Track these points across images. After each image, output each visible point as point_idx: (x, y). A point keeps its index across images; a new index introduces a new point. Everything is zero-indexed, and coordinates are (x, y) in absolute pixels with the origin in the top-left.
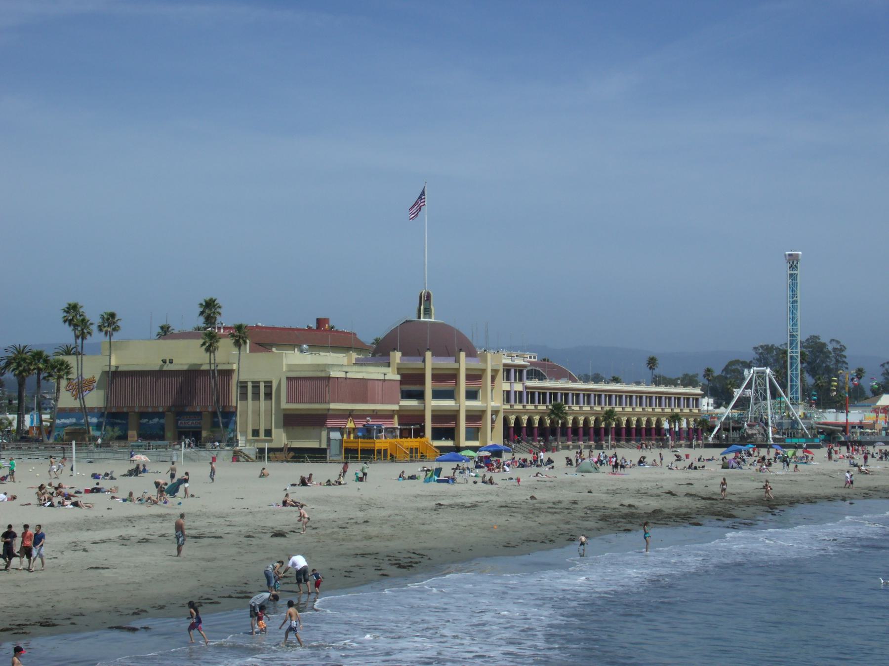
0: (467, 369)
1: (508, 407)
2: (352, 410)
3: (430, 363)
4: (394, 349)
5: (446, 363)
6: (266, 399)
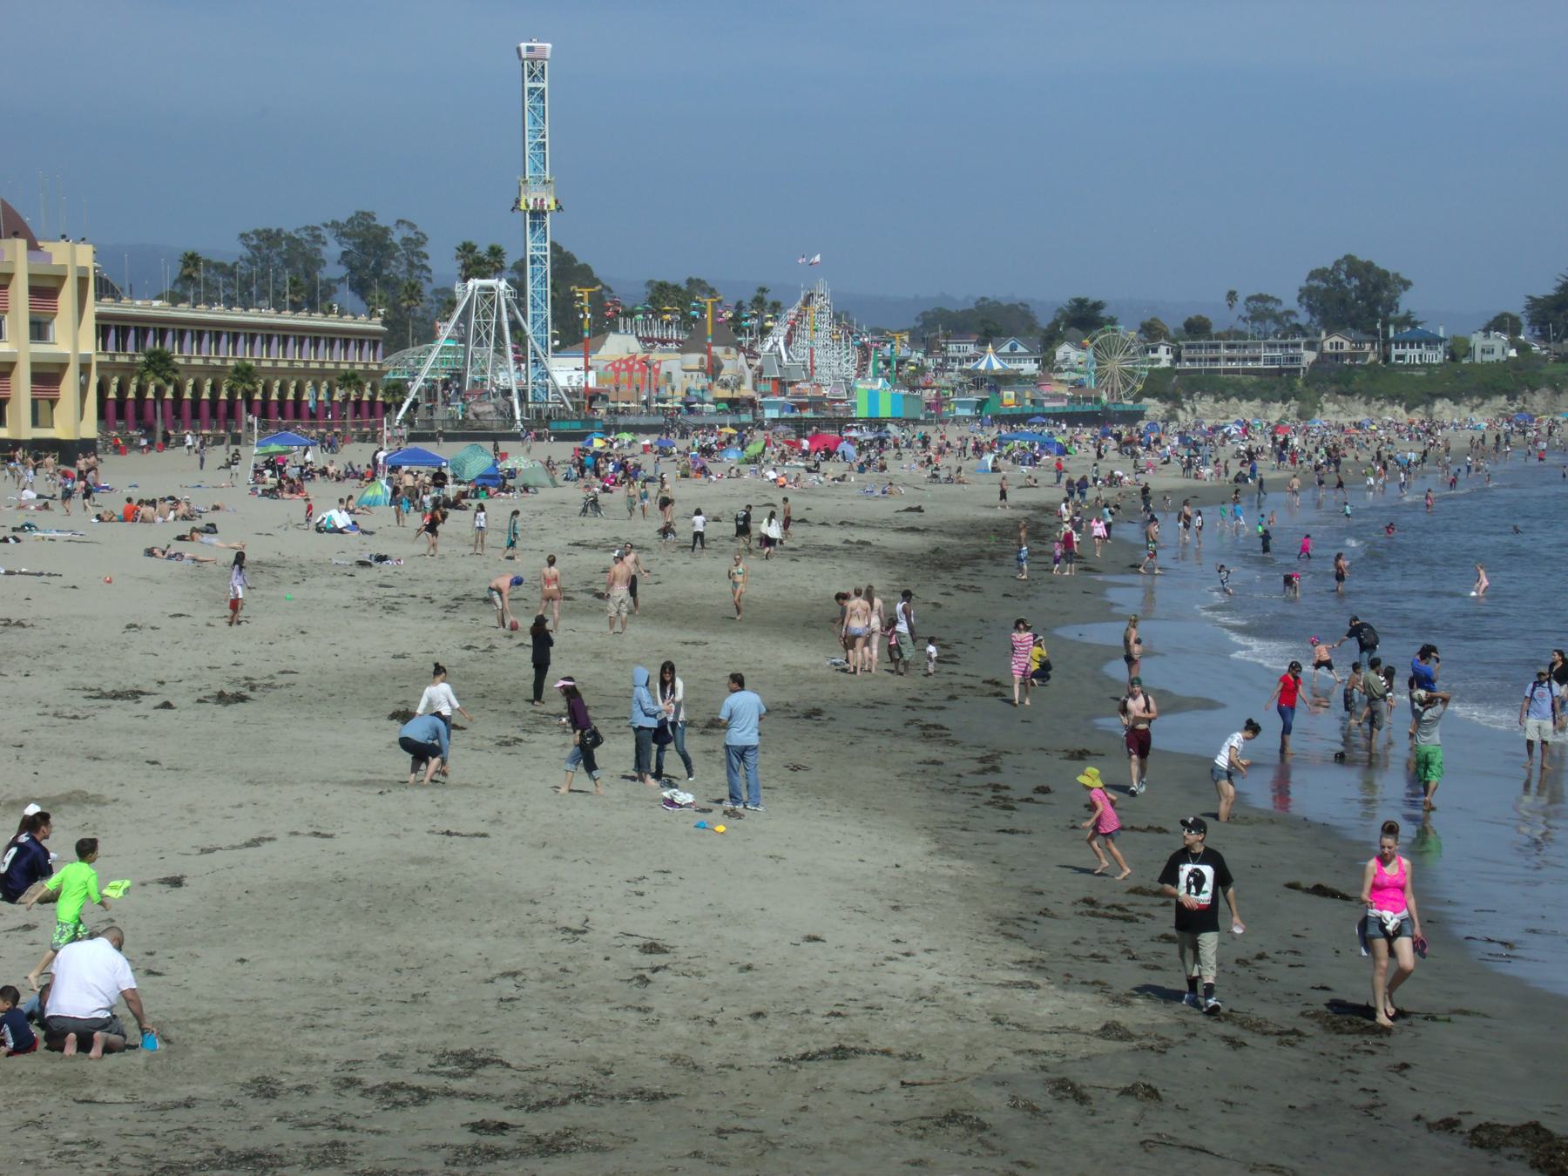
0: (31, 276)
1: (107, 359)
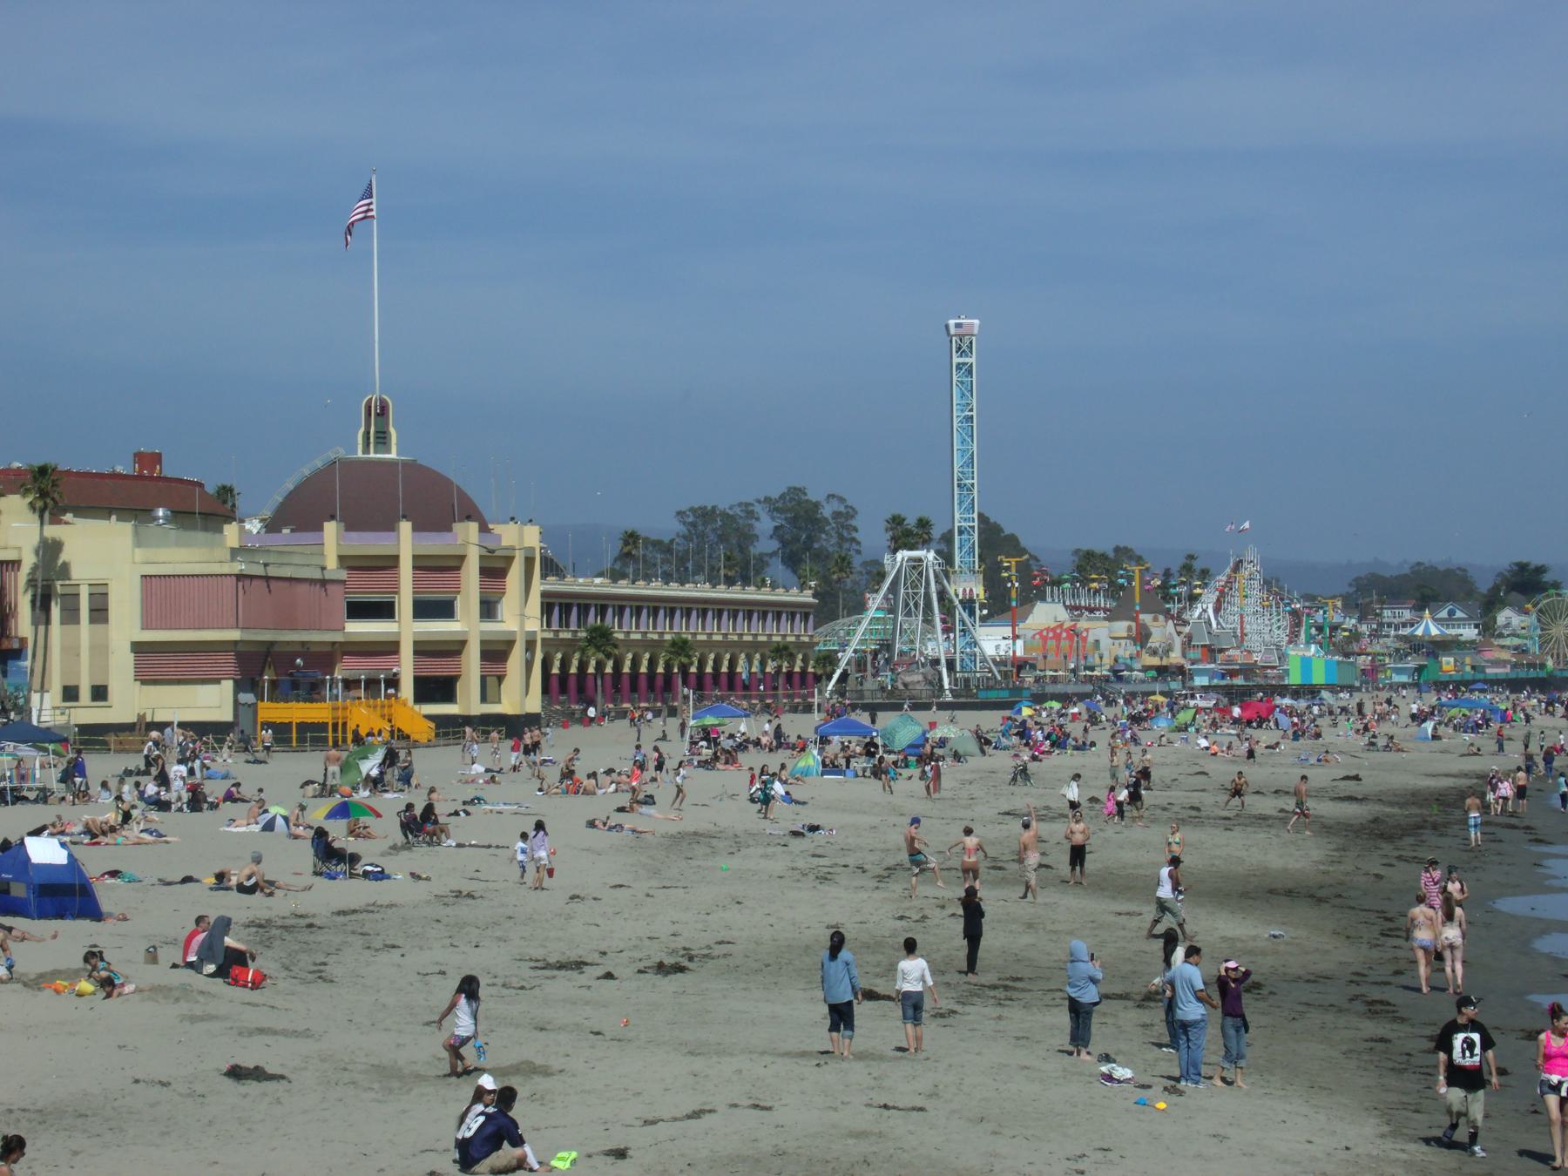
2: (272, 643)
3: (406, 541)
4: (333, 517)
5: (370, 544)
6: (92, 621)
